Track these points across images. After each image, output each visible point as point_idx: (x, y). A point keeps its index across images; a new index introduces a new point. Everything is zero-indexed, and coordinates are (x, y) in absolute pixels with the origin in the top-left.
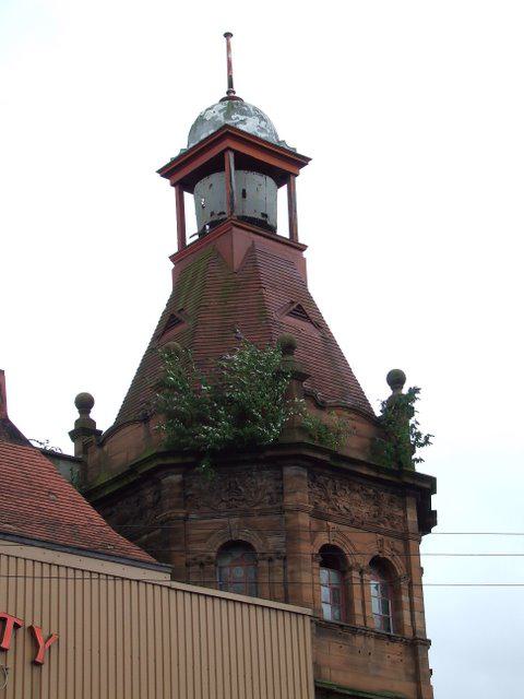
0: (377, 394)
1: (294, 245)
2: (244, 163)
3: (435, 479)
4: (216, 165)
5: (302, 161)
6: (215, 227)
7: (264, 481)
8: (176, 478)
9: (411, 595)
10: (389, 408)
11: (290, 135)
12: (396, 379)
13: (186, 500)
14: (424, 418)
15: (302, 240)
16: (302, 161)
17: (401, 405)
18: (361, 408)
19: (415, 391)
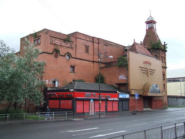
0: (163, 44)
1: (155, 29)
2: (153, 23)
3: (22, 39)
4: (151, 23)
5: (156, 22)
6: (149, 28)
7: (158, 51)
8: (152, 50)
9: (165, 60)
10: (45, 30)
11: (155, 20)
12: (165, 43)
13: (153, 52)
14: (167, 46)
15: (156, 29)
16: (156, 22)
17: (165, 45)
18: (161, 45)
19: (167, 44)
